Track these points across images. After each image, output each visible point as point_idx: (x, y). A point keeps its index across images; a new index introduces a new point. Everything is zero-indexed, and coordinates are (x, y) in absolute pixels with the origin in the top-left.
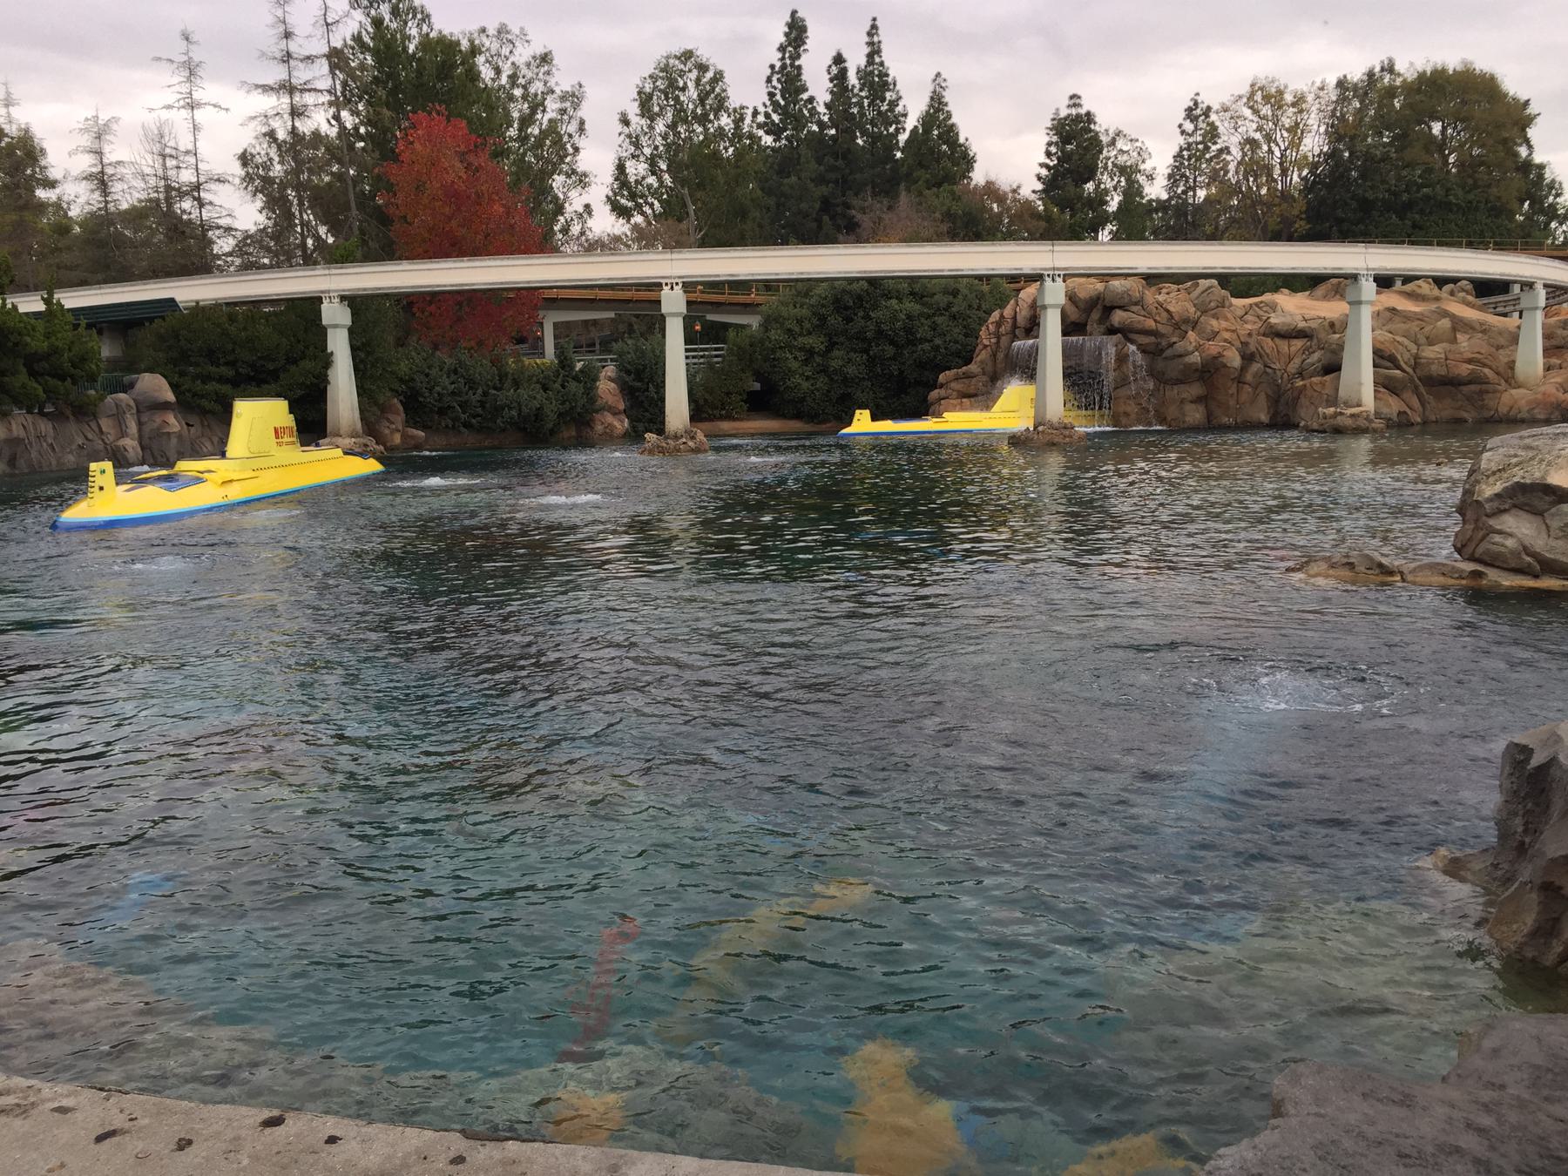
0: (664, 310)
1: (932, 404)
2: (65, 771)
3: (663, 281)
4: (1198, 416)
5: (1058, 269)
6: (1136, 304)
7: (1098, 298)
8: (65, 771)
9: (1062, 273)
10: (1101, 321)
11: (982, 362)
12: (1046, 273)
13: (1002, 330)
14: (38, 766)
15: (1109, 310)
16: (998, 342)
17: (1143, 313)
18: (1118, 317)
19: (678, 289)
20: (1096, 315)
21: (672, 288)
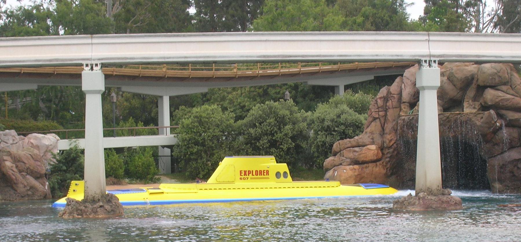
0: (84, 89)
1: (327, 170)
2: (151, 194)
3: (84, 63)
4: (516, 135)
5: (434, 56)
6: (505, 84)
7: (473, 79)
8: (151, 194)
9: (437, 59)
10: (475, 99)
11: (372, 133)
12: (423, 59)
13: (389, 104)
14: (486, 28)
15: (481, 89)
16: (386, 115)
17: (511, 92)
18: (490, 95)
19: (97, 70)
20: (471, 93)
21: (92, 69)
